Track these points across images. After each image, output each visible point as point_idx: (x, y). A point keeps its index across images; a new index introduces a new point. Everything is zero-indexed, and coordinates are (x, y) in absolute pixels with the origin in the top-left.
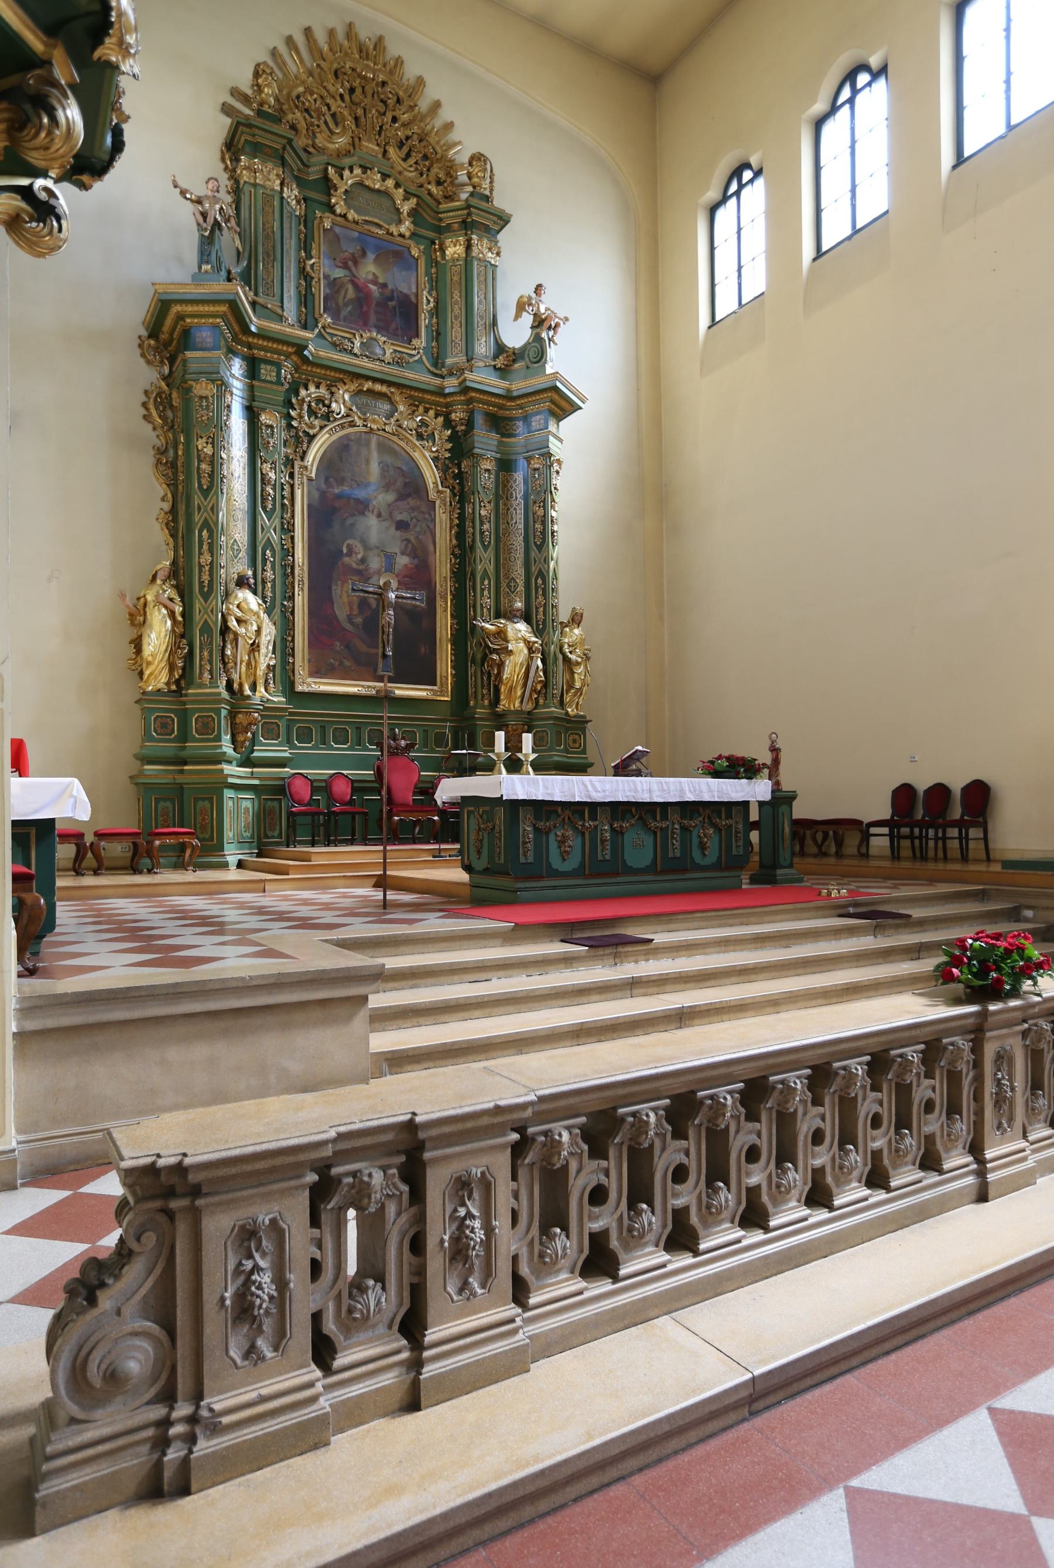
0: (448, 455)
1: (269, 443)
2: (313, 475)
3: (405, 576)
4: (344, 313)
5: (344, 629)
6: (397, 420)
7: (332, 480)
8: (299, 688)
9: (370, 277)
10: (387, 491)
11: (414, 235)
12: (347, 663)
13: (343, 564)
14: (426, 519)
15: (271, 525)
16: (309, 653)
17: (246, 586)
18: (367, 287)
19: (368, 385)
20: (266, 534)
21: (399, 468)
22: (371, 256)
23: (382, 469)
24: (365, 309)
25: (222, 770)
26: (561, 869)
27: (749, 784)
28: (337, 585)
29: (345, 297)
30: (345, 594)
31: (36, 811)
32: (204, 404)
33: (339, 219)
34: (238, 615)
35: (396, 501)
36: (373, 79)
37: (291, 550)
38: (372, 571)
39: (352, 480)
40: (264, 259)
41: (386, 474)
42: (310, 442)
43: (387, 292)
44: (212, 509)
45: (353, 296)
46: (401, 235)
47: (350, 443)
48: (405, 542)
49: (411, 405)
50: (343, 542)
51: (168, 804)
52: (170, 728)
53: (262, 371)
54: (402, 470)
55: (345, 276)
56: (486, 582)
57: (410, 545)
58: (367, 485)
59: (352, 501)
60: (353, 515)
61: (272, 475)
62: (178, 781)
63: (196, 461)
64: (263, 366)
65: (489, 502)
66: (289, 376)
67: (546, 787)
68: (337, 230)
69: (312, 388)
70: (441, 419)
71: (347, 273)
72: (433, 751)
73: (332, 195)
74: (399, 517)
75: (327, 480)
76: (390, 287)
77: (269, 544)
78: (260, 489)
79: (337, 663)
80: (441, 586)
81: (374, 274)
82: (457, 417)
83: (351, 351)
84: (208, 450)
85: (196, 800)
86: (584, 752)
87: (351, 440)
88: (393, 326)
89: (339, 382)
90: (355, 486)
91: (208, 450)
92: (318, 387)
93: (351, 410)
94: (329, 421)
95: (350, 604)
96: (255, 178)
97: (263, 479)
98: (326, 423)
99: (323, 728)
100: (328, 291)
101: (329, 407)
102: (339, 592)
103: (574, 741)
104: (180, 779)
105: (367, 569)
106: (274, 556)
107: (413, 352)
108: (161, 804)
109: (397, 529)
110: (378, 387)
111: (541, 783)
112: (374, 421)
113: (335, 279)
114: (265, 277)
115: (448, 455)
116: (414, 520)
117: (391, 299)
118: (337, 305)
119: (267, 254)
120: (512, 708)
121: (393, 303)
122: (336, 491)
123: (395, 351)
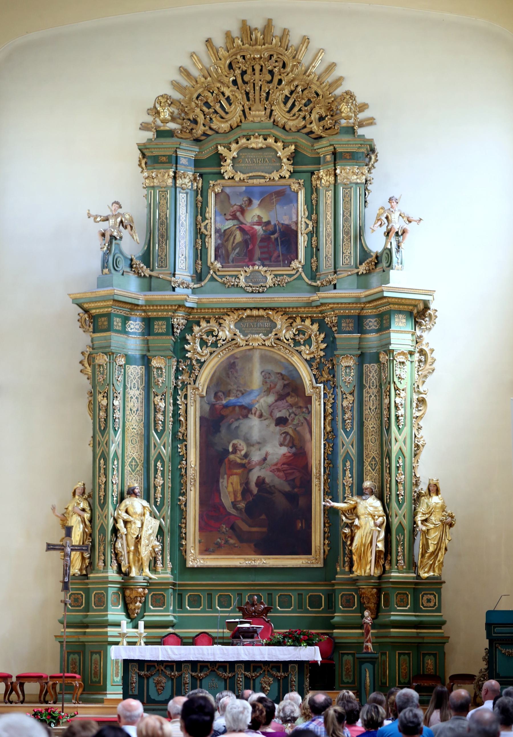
0: (322, 354)
1: (158, 381)
2: (204, 393)
3: (284, 464)
4: (232, 256)
5: (229, 514)
6: (276, 334)
7: (220, 394)
8: (190, 564)
9: (256, 219)
10: (268, 395)
11: (293, 174)
12: (232, 541)
13: (229, 460)
14: (303, 412)
15: (161, 443)
16: (200, 536)
17: (133, 495)
18: (253, 228)
19: (248, 312)
20: (158, 449)
21: (279, 373)
22: (256, 202)
23: (263, 376)
24: (250, 247)
25: (107, 632)
26: (157, 699)
27: (295, 650)
28: (223, 479)
29: (233, 242)
30: (230, 485)
31: (289, 658)
32: (102, 369)
33: (230, 181)
34: (125, 518)
35: (276, 401)
36: (261, 58)
37: (185, 455)
38: (254, 463)
39: (237, 391)
40: (159, 240)
41: (268, 380)
42: (200, 367)
43: (271, 228)
44: (106, 444)
45: (241, 240)
46: (281, 177)
47: (236, 360)
48: (284, 435)
49: (289, 318)
50: (229, 443)
51: (76, 656)
52: (80, 601)
53: (156, 327)
54: (281, 374)
55: (234, 225)
56: (348, 464)
57: (288, 437)
58: (250, 393)
59: (237, 409)
60: (237, 419)
61: (162, 405)
62: (81, 640)
63: (98, 409)
64: (156, 323)
65: (351, 393)
66: (182, 321)
67: (140, 652)
68: (227, 190)
69: (203, 324)
70: (315, 327)
71: (235, 222)
72: (308, 612)
73: (222, 166)
74: (278, 415)
75: (216, 394)
76: (273, 223)
77: (159, 457)
78: (153, 416)
79: (223, 542)
80: (316, 470)
81: (258, 216)
82: (328, 321)
83: (237, 285)
84: (104, 402)
85: (92, 653)
86: (439, 610)
87: (237, 358)
88: (275, 255)
89: (224, 315)
90: (240, 395)
91: (104, 402)
92: (208, 322)
93: (235, 335)
94: (217, 347)
95: (235, 493)
96: (153, 182)
97: (155, 408)
98: (215, 349)
99: (210, 595)
100: (219, 242)
101: (217, 336)
102: (225, 483)
103: (429, 601)
104: (83, 639)
105: (249, 463)
106: (163, 466)
107: (294, 272)
108: (72, 656)
109: (277, 424)
110: (255, 313)
111: (160, 649)
112: (255, 340)
113: (225, 231)
114: (160, 254)
115: (322, 354)
116: (293, 415)
117: (273, 233)
118: (227, 251)
119: (162, 236)
120: (363, 574)
121: (276, 235)
122: (224, 402)
123: (276, 276)
